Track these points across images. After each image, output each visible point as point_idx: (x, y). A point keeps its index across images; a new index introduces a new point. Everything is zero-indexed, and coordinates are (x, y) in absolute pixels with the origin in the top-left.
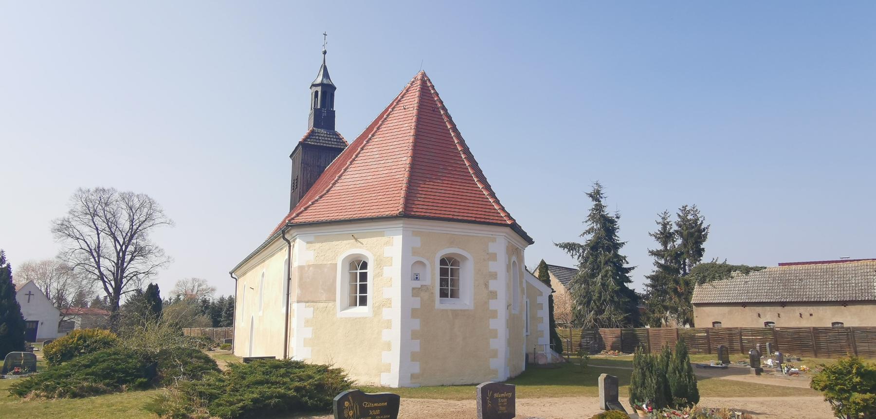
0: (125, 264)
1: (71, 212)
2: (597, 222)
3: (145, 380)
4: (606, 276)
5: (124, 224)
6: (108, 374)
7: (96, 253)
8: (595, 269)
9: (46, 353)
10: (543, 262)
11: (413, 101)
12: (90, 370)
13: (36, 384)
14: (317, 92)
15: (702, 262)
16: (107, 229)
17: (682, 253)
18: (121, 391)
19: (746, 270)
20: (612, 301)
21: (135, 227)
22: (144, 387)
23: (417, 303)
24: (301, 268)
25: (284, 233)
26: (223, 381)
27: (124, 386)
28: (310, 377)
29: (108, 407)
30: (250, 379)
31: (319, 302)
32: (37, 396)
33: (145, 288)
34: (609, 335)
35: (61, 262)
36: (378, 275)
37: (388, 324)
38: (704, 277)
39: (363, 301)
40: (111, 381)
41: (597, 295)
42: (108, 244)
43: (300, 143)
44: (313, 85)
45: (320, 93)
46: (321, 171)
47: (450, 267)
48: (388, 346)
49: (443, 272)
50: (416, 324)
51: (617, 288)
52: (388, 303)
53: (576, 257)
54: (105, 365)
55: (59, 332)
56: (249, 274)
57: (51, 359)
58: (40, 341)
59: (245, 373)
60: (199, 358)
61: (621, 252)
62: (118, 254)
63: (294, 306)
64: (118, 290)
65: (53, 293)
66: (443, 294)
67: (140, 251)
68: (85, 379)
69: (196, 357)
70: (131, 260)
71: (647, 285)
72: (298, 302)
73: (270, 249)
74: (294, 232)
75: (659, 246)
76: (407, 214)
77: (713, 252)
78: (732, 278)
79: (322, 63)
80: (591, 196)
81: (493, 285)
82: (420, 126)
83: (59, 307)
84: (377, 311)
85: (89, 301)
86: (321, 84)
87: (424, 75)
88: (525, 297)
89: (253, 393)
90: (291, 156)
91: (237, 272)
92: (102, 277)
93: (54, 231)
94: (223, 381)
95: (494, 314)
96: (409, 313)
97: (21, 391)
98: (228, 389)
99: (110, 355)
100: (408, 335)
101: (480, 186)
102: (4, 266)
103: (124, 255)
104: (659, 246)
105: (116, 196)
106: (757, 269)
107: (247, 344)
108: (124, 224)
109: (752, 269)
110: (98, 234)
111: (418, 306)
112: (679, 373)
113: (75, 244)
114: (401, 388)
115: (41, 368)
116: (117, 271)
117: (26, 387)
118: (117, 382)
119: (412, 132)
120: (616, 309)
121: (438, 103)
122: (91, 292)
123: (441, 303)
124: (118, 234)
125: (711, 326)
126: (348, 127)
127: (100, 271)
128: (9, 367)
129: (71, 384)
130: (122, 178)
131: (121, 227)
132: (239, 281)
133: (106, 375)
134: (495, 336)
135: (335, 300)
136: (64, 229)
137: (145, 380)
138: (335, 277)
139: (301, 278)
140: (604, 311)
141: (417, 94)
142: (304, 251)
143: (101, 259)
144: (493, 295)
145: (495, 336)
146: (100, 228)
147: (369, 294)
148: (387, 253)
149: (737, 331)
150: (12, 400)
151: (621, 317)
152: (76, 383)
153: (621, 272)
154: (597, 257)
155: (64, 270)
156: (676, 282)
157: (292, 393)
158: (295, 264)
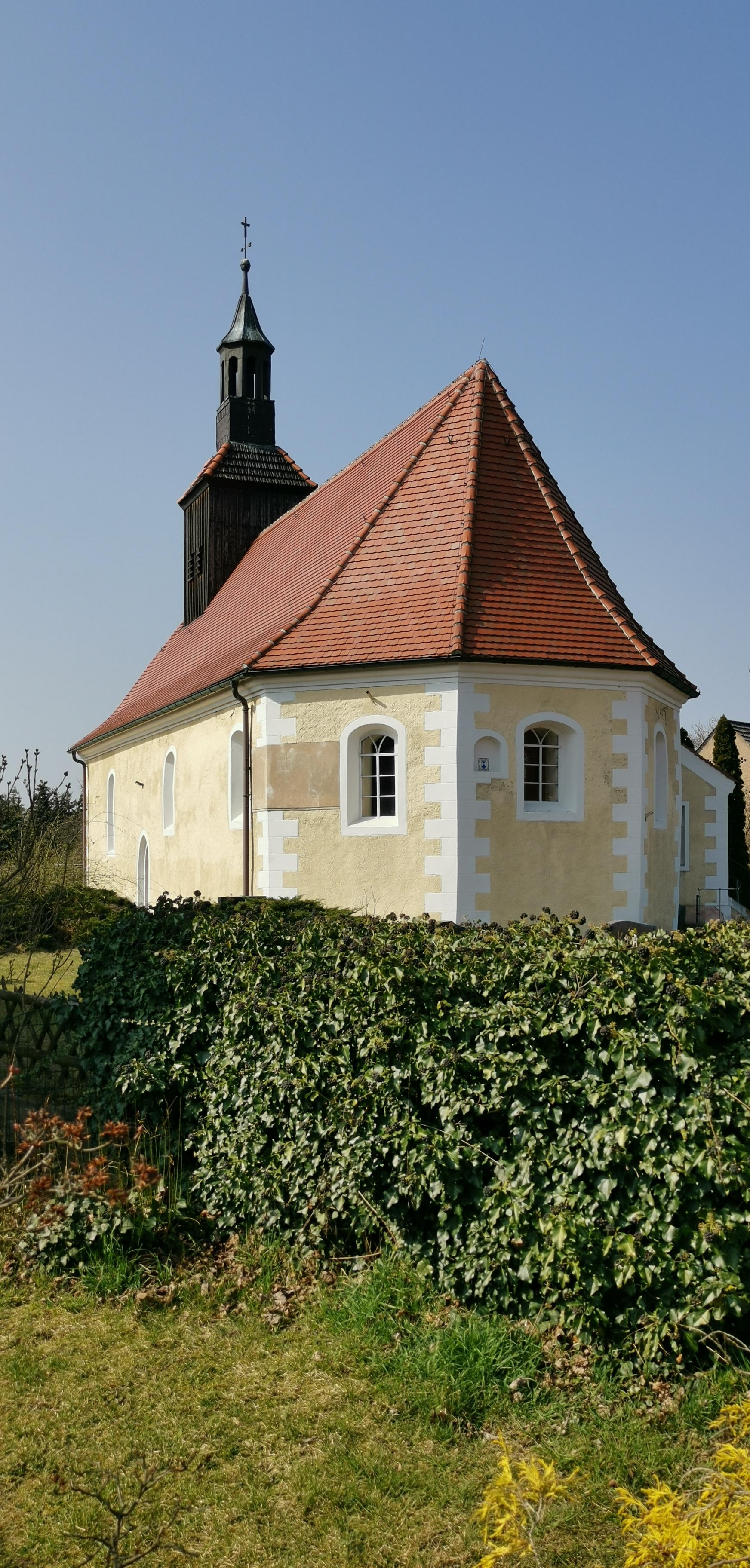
10: (723, 718)
11: (466, 423)
14: (233, 361)
23: (484, 810)
24: (273, 749)
25: (235, 685)
31: (309, 808)
36: (415, 762)
37: (436, 847)
39: (388, 808)
43: (204, 479)
45: (240, 363)
47: (541, 746)
49: (531, 755)
50: (484, 847)
52: (433, 811)
63: (262, 817)
66: (531, 794)
72: (270, 809)
74: (255, 685)
76: (465, 655)
79: (240, 291)
82: (482, 480)
84: (415, 823)
86: (243, 343)
87: (487, 369)
88: (679, 797)
90: (182, 503)
95: (621, 830)
96: (471, 828)
101: (596, 592)
107: (262, 846)
119: (469, 493)
121: (513, 427)
123: (527, 809)
132: (91, 766)
134: (623, 869)
135: (337, 806)
138: (337, 767)
139: (273, 767)
141: (475, 411)
142: (273, 719)
144: (620, 795)
145: (623, 869)
147: (399, 795)
148: (430, 723)
158: (260, 741)
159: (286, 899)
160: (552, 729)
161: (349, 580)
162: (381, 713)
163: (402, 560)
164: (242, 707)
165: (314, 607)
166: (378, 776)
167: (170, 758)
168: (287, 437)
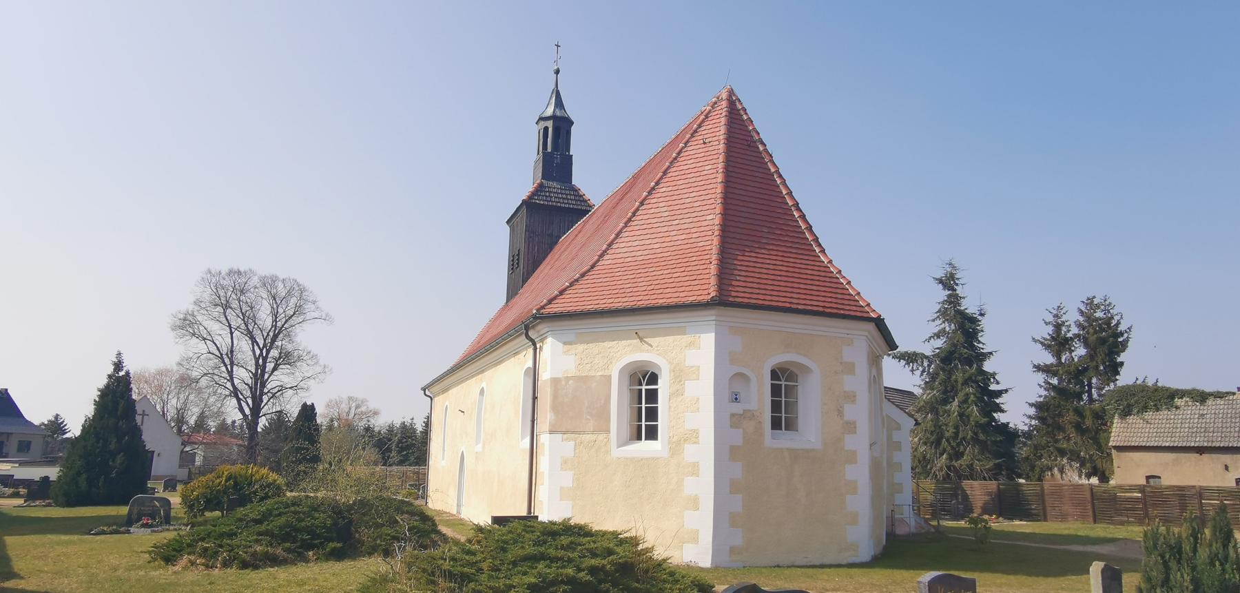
0: (266, 376)
1: (197, 303)
2: (950, 321)
3: (339, 545)
4: (965, 401)
5: (265, 318)
6: (288, 534)
7: (228, 359)
8: (948, 393)
9: (185, 498)
11: (717, 130)
12: (263, 528)
13: (189, 545)
14: (546, 129)
15: (1119, 383)
16: (243, 327)
17: (1086, 370)
18: (307, 561)
19: (1201, 397)
20: (975, 440)
21: (279, 324)
22: (338, 555)
24: (555, 381)
25: (527, 328)
26: (474, 554)
27: (311, 553)
28: (610, 552)
29: (299, 585)
30: (515, 552)
31: (584, 432)
32: (193, 563)
33: (293, 411)
34: (978, 491)
35: (183, 370)
37: (694, 469)
38: (1129, 406)
39: (652, 434)
40: (293, 546)
41: (952, 430)
42: (244, 347)
43: (524, 202)
44: (541, 119)
46: (552, 242)
47: (783, 383)
48: (694, 503)
49: (776, 390)
50: (737, 470)
51: (984, 420)
52: (693, 436)
53: (918, 373)
54: (283, 520)
55: (180, 467)
56: (453, 391)
57: (191, 507)
58: (158, 478)
59: (506, 542)
60: (412, 514)
61: (988, 366)
62: (257, 360)
63: (544, 439)
64: (256, 410)
65: (171, 413)
66: (776, 424)
67: (286, 358)
68: (257, 541)
69: (407, 512)
70: (275, 369)
71: (1030, 417)
72: (551, 432)
73: (495, 354)
74: (543, 328)
75: (1048, 359)
76: (722, 301)
77: (1135, 368)
78: (1177, 408)
79: (553, 86)
80: (940, 281)
81: (850, 412)
83: (180, 431)
84: (676, 448)
85: (212, 424)
86: (553, 117)
87: (731, 93)
89: (525, 574)
90: (508, 222)
91: (431, 389)
92: (235, 393)
93: (174, 328)
94: (474, 554)
95: (851, 458)
96: (726, 454)
97: (168, 555)
98: (485, 566)
99: (287, 506)
100: (725, 487)
102: (121, 374)
103: (265, 359)
104: (1048, 359)
105: (255, 281)
106: (1219, 395)
107: (453, 493)
108: (265, 318)
109: (1211, 394)
110: (232, 333)
111: (739, 441)
112: (1222, 564)
113: (202, 347)
114: (715, 568)
115: (177, 519)
116: (256, 384)
117: (174, 550)
118: (301, 547)
119: (720, 177)
120: (982, 452)
121: (754, 134)
122: (219, 413)
124: (257, 333)
125: (1144, 482)
126: (593, 177)
127: (233, 385)
128: (134, 517)
129: (238, 547)
130: (264, 258)
131: (259, 322)
133: (286, 535)
136: (187, 325)
137: (339, 545)
139: (555, 397)
140: (962, 454)
141: (723, 120)
142: (557, 356)
143: (235, 368)
144: (851, 427)
146: (233, 324)
147: (662, 423)
148: (691, 362)
149: (1194, 491)
150: (155, 569)
151: (990, 465)
152: (246, 547)
153: (989, 399)
154: (950, 373)
155: (186, 382)
156: (1079, 412)
157: (584, 576)
158: (545, 375)
159: (554, 523)
160: (792, 369)
161: (623, 245)
162: (648, 351)
163: (666, 229)
164: (531, 351)
165: (593, 266)
166: (644, 405)
167: (482, 392)
168: (579, 179)
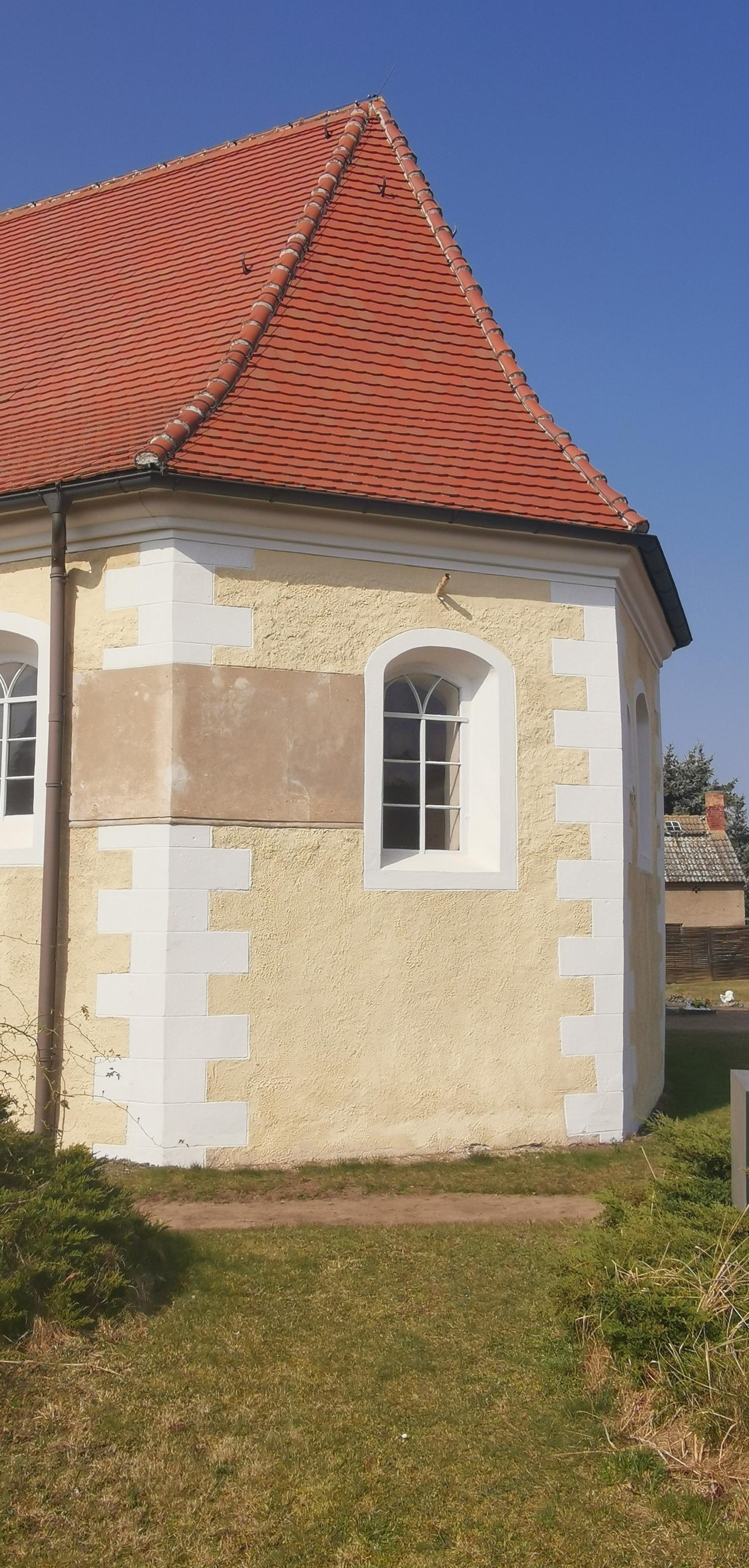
31: (282, 824)
37: (580, 920)
48: (581, 995)
135: (357, 823)
162: (458, 627)
